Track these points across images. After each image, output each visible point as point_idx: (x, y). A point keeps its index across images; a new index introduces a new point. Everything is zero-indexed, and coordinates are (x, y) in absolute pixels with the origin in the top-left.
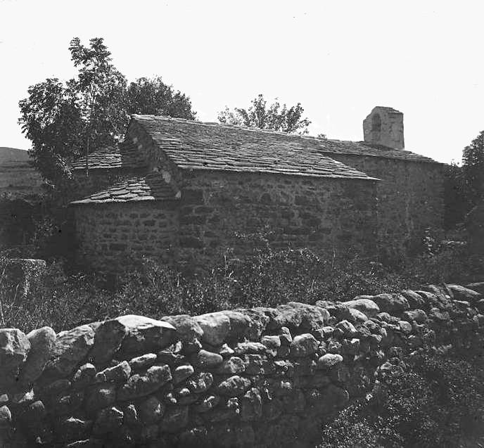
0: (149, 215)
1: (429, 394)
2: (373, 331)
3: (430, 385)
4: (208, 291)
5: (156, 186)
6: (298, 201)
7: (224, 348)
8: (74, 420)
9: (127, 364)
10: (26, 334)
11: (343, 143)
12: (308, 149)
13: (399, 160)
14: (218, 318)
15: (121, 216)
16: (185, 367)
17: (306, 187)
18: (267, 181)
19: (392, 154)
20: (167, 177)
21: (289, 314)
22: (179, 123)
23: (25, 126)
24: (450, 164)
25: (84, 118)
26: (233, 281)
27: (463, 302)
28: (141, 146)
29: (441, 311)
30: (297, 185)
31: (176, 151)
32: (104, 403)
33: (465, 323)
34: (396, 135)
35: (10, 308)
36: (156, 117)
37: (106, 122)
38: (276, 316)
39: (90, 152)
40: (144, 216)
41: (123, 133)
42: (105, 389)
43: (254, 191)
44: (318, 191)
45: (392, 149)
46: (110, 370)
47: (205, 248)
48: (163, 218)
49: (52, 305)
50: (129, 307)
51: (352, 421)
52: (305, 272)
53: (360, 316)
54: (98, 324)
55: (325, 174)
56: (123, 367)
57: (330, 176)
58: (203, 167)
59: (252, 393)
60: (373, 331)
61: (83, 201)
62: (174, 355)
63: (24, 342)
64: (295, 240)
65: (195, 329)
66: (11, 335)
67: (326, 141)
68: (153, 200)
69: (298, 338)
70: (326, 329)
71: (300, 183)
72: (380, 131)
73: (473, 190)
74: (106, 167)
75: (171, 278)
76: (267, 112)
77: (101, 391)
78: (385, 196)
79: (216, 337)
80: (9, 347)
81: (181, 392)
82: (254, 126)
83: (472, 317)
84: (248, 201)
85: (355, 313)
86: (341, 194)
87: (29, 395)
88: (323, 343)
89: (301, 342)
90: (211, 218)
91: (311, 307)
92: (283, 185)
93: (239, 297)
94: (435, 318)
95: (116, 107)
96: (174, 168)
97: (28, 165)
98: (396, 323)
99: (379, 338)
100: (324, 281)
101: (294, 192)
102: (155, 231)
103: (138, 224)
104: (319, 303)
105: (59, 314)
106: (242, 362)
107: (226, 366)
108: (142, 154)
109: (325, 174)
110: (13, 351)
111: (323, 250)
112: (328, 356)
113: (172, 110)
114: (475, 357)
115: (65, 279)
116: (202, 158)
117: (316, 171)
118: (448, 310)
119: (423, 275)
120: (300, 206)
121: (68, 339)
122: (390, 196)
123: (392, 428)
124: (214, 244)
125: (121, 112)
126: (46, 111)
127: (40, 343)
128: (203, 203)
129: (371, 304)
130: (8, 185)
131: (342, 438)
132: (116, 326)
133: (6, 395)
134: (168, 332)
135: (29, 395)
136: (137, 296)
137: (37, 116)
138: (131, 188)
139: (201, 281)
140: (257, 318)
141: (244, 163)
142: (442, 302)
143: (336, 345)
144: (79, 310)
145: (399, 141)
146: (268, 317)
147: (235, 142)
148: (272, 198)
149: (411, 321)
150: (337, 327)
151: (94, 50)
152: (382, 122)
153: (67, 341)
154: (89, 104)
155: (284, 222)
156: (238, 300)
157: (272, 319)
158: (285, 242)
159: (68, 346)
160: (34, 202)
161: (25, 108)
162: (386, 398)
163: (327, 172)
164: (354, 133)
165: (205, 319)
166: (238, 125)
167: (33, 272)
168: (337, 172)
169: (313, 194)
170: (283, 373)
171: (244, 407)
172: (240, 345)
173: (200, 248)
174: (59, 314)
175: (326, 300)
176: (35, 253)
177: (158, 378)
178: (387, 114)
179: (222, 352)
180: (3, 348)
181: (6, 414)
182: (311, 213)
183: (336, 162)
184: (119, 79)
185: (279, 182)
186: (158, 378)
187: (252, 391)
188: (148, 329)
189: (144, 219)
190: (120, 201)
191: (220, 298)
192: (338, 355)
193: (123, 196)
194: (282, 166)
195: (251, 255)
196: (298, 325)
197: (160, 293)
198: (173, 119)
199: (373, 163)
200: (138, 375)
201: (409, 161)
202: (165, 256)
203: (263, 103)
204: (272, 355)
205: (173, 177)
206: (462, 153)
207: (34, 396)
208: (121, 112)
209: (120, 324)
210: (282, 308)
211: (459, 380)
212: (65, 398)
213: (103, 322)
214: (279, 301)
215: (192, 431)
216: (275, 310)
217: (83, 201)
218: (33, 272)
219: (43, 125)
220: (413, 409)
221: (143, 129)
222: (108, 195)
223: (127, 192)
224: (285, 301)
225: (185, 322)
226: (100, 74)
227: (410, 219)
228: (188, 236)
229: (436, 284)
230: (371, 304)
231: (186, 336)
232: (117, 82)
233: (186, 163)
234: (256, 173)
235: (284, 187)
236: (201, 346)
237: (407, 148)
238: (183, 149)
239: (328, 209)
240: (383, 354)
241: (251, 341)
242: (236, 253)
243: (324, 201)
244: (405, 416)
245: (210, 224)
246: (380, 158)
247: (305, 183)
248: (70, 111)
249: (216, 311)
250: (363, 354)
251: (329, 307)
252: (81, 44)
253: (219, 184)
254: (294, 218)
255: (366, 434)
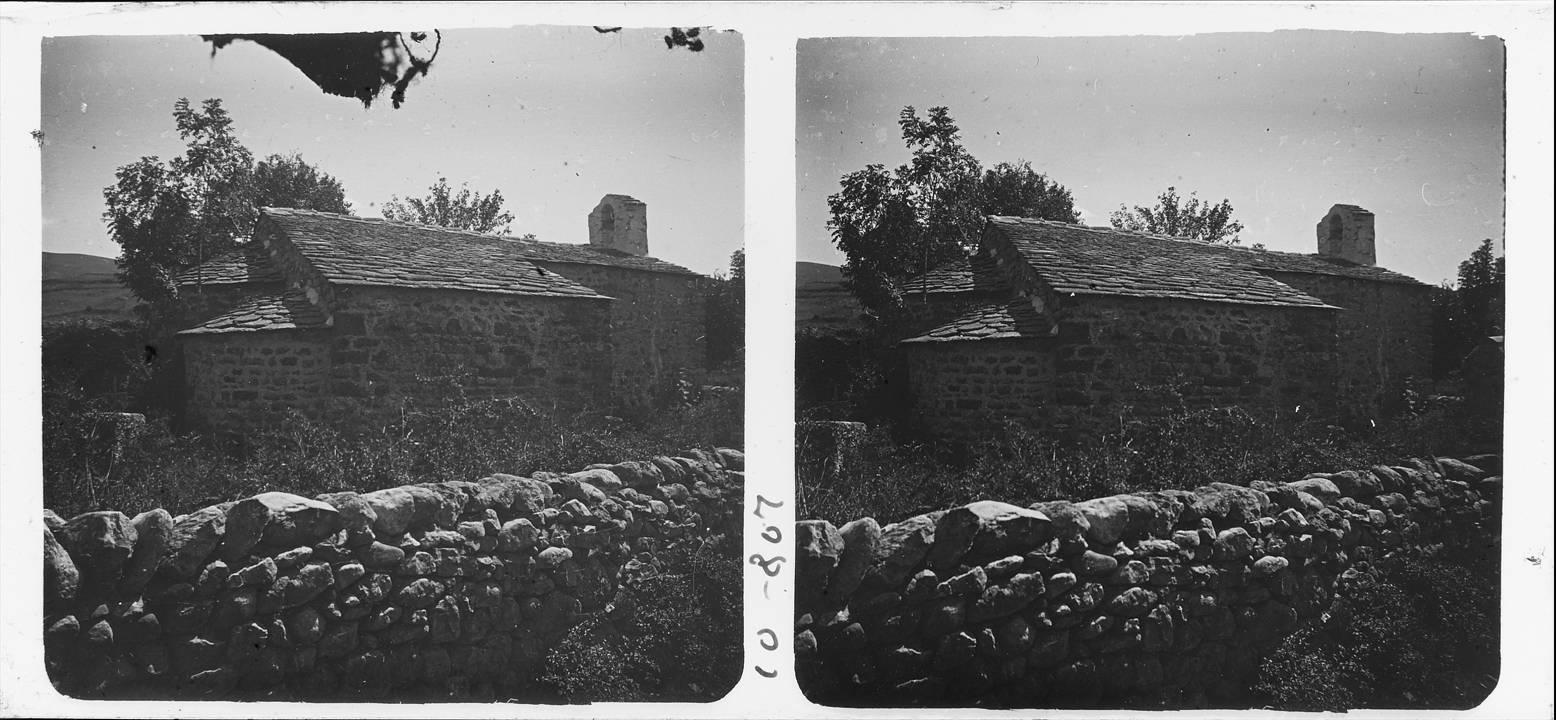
0: (1013, 358)
1: (1411, 614)
2: (1331, 524)
3: (1413, 600)
4: (1097, 466)
5: (1023, 316)
6: (1225, 338)
7: (406, 539)
8: (906, 650)
9: (272, 561)
10: (838, 528)
11: (561, 246)
12: (1240, 264)
13: (1369, 281)
14: (1111, 506)
15: (973, 360)
16: (1064, 575)
17: (1237, 319)
18: (1180, 310)
19: (1359, 272)
20: (1038, 304)
21: (497, 491)
22: (328, 219)
23: (837, 232)
24: (1441, 286)
25: (194, 212)
26: (1132, 453)
27: (1459, 483)
28: (1002, 260)
29: (1428, 494)
30: (496, 307)
31: (1051, 268)
32: (240, 616)
33: (1462, 512)
34: (1364, 245)
35: (816, 490)
36: (296, 211)
37: (951, 226)
38: (477, 493)
39: (929, 270)
40: (1006, 359)
41: (975, 242)
42: (950, 606)
43: (1162, 325)
44: (1253, 325)
45: (1359, 265)
46: (957, 578)
47: (1092, 406)
48: (309, 354)
49: (874, 486)
50: (985, 490)
51: (1302, 652)
52: (1234, 440)
53: (1312, 503)
54: (940, 514)
55: (1263, 301)
56: (976, 574)
57: (1270, 303)
58: (1090, 291)
59: (1159, 612)
60: (614, 515)
61: (918, 339)
62: (1048, 558)
63: (835, 539)
64: (494, 385)
65: (1078, 522)
66: (817, 529)
67: (1264, 253)
68: (1018, 338)
69: (1225, 533)
70: (549, 512)
71: (1228, 314)
72: (1341, 239)
73: (1474, 323)
74: (952, 291)
75: (1044, 448)
76: (451, 203)
77: (236, 600)
78: (1348, 332)
79: (395, 523)
80: (109, 537)
81: (1059, 611)
82: (1162, 232)
83: (1471, 503)
84: (429, 330)
85: (1307, 498)
86: (1286, 329)
87: (843, 615)
88: (1261, 541)
89: (1229, 539)
90: (1101, 362)
91: (1243, 490)
92: (1204, 315)
93: (1141, 476)
94: (1420, 506)
95: (966, 205)
96: (322, 283)
97: (841, 287)
98: (1364, 513)
99: (1340, 533)
100: (1261, 453)
101: (1219, 327)
102: (1022, 382)
103: (997, 371)
104: (1254, 483)
105: (885, 499)
106: (1145, 567)
107: (1122, 574)
108: (1003, 272)
109: (1263, 301)
110: (819, 551)
111: (1260, 408)
112: (1268, 559)
113: (1045, 209)
114: (1476, 561)
115: (893, 450)
116: (362, 268)
117: (1250, 297)
118: (1439, 493)
119: (1402, 445)
120: (1228, 346)
121: (899, 535)
122: (1355, 331)
123: (643, 653)
124: (1105, 401)
125: (973, 213)
126: (866, 211)
127: (151, 531)
128: (365, 333)
129: (609, 476)
130: (812, 316)
131: (1287, 676)
132: (966, 516)
133: (105, 606)
134: (329, 516)
135: (843, 615)
136: (995, 474)
137: (129, 210)
138: (988, 320)
139: (1087, 452)
140: (1166, 505)
141: (421, 276)
142: (1429, 482)
143: (1279, 543)
144: (913, 495)
145: (1368, 254)
146: (466, 495)
147: (408, 245)
148: (461, 325)
149: (1384, 510)
150: (1280, 518)
151: (934, 123)
152: (1344, 226)
153: (896, 538)
154: (927, 200)
155: (1205, 368)
156: (423, 471)
157: (1187, 507)
158: (1207, 397)
159: (898, 545)
160: (850, 340)
161: (837, 208)
162: (634, 609)
163: (539, 289)
164: (575, 232)
165: (1092, 507)
166: (1139, 231)
167: (848, 440)
168: (553, 289)
169: (1247, 328)
170: (1203, 583)
171: (1147, 632)
172: (1142, 543)
173: (1086, 405)
174: (885, 499)
175: (1264, 480)
176: (851, 412)
177: (1025, 590)
178: (622, 205)
179: (404, 544)
180: (806, 548)
181: (106, 633)
182: (518, 346)
183: (1279, 284)
184: (970, 165)
185: (471, 302)
186: (1025, 590)
187: (1159, 609)
188: (1012, 520)
189: (1006, 365)
190: (971, 338)
191: (1113, 477)
192: (566, 549)
193: (976, 332)
194: (476, 280)
195: (1157, 415)
196: (1225, 515)
197: (1029, 470)
198: (1046, 222)
199: (1331, 285)
200: (996, 586)
201: (1383, 282)
202: (1035, 418)
203: (446, 190)
204: (1187, 558)
205: (1047, 305)
206: (1457, 271)
207: (849, 617)
208: (973, 213)
209: (261, 504)
210: (1202, 491)
211: (1454, 593)
212: (186, 609)
213: (948, 511)
214: (1198, 480)
215: (1074, 666)
216: (1192, 494)
217: (918, 339)
218: (848, 440)
219: (863, 231)
220: (1388, 635)
221: (1003, 236)
222: (954, 330)
223: (982, 325)
224: (488, 472)
225: (1064, 511)
226: (943, 159)
227: (1384, 365)
228: (1069, 389)
229: (1421, 457)
230: (609, 476)
231: (1065, 531)
232: (967, 169)
233: (1066, 284)
234: (1165, 298)
235: (1205, 319)
236: (1086, 545)
237: (651, 254)
238: (1061, 265)
239: (1267, 350)
240: (1346, 557)
241: (1158, 537)
242: (1137, 413)
243: (535, 330)
244: (660, 635)
245: (1100, 371)
246: (1343, 278)
247: (1234, 313)
248: (900, 211)
249: (1108, 496)
250: (1317, 555)
251: (551, 481)
252: (915, 116)
253: (1113, 315)
254: (1218, 364)
255: (1320, 670)
